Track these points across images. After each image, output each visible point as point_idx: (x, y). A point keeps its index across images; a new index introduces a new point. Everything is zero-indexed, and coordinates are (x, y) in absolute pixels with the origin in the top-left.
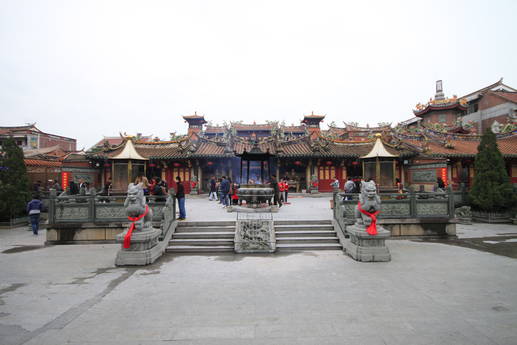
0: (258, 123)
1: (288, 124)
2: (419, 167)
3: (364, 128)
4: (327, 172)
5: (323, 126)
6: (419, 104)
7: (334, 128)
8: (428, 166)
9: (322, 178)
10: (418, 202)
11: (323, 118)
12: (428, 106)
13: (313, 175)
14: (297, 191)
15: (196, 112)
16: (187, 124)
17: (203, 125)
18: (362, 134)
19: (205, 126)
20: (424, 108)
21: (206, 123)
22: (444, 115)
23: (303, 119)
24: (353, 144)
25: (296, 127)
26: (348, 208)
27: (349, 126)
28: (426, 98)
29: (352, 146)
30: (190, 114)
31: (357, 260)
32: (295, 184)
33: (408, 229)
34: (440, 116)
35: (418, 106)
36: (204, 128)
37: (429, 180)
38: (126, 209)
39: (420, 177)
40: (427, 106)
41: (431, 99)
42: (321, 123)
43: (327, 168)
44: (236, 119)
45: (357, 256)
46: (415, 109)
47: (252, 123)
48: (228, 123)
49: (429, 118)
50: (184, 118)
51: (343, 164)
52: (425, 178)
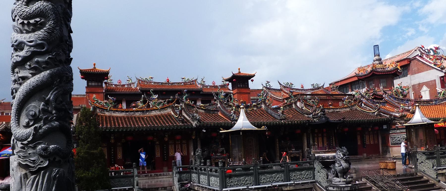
0: (172, 81)
2: (398, 131)
3: (299, 90)
5: (252, 85)
15: (239, 69)
23: (230, 76)
39: (399, 140)
44: (145, 76)
47: (164, 81)
48: (134, 80)
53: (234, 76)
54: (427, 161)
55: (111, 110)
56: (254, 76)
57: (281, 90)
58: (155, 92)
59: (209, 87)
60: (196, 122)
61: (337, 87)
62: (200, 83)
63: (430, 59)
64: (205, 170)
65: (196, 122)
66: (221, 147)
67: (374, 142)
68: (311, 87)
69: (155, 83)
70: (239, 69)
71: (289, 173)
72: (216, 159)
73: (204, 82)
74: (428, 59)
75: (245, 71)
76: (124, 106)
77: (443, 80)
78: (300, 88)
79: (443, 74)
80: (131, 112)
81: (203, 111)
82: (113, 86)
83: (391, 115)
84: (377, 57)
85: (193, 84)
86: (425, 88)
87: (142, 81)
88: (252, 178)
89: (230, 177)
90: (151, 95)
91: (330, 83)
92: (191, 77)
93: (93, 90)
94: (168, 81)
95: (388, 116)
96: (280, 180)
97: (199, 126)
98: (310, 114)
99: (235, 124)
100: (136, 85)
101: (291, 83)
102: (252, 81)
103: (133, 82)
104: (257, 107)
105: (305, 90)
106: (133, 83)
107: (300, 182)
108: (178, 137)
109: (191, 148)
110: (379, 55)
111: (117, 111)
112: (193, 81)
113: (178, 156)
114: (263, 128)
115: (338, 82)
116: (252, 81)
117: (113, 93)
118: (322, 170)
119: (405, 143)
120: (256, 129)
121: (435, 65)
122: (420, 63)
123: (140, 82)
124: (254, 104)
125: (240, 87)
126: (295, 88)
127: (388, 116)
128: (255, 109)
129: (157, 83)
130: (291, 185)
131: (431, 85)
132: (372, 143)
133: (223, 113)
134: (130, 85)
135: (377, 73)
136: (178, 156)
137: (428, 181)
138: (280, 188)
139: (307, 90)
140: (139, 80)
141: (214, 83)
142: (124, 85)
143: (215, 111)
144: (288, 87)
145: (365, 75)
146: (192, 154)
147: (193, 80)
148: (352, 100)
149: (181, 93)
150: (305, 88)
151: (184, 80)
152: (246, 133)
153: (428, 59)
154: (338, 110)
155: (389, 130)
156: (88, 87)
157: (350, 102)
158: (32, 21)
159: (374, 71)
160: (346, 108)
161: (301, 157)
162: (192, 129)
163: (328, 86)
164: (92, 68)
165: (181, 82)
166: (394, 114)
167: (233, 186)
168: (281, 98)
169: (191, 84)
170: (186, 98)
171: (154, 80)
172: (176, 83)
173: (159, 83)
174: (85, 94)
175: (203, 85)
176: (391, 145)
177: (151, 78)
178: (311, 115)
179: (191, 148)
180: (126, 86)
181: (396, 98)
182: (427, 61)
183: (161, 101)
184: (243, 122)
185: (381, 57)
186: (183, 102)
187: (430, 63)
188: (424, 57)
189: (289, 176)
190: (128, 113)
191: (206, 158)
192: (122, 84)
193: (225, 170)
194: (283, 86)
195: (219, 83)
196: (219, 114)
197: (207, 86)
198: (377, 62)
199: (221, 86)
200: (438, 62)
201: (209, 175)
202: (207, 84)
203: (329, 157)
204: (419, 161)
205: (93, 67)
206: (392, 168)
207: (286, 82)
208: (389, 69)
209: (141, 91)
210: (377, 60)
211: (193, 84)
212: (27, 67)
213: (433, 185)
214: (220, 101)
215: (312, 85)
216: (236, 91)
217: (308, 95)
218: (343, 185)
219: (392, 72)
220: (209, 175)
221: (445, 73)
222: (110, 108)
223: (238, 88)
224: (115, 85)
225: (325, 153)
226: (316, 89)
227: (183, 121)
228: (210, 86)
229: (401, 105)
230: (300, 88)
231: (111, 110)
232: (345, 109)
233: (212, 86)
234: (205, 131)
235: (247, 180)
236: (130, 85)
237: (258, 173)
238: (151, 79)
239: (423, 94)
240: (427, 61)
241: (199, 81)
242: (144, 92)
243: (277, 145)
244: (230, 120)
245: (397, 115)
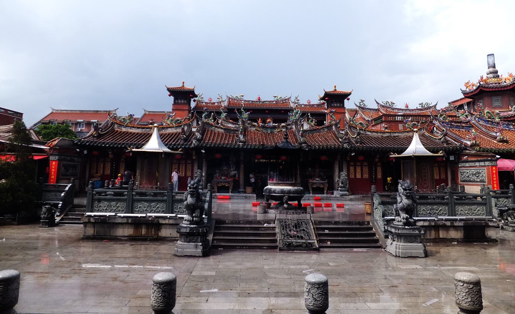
0: (263, 99)
1: (303, 101)
2: (467, 165)
3: (402, 110)
4: (359, 170)
5: (349, 104)
6: (468, 83)
7: (363, 108)
8: (477, 164)
9: (352, 176)
10: (456, 204)
11: (350, 94)
12: (479, 86)
13: (342, 173)
14: (325, 192)
15: (183, 83)
16: (172, 98)
17: (192, 100)
18: (400, 118)
19: (194, 101)
20: (475, 88)
21: (196, 96)
22: (499, 98)
23: (322, 95)
24: (389, 134)
25: (313, 105)
26: (386, 209)
27: (383, 106)
28: (476, 74)
29: (388, 137)
30: (176, 84)
31: (396, 256)
32: (323, 184)
33: (448, 233)
34: (494, 98)
35: (467, 84)
36: (193, 105)
37: (479, 180)
38: (185, 203)
39: (468, 177)
40: (478, 84)
41: (482, 78)
42: (346, 101)
43: (359, 164)
44: (235, 94)
45: (396, 251)
46: (464, 88)
47: (255, 99)
48: (224, 98)
49: (482, 101)
50: (169, 90)
51: (377, 160)
52: (475, 178)
56: (350, 94)
58: (247, 110)
62: (293, 101)
67: (440, 177)
69: (245, 101)
70: (183, 83)
71: (455, 206)
72: (219, 182)
75: (341, 89)
78: (404, 107)
81: (222, 131)
82: (204, 104)
83: (462, 143)
84: (491, 70)
85: (286, 102)
89: (99, 201)
91: (450, 101)
92: (282, 95)
93: (179, 107)
94: (259, 100)
95: (458, 144)
96: (160, 211)
97: (198, 146)
101: (392, 102)
102: (348, 99)
103: (223, 100)
104: (287, 128)
105: (409, 110)
106: (223, 101)
107: (429, 218)
110: (494, 67)
111: (133, 127)
113: (175, 176)
114: (440, 154)
115: (458, 101)
116: (348, 99)
118: (379, 207)
120: (431, 154)
126: (396, 107)
127: (458, 144)
128: (284, 130)
130: (171, 218)
132: (359, 176)
135: (486, 90)
136: (175, 176)
137: (374, 235)
138: (156, 220)
139: (413, 110)
140: (230, 98)
142: (214, 103)
143: (236, 130)
145: (472, 92)
148: (418, 122)
151: (276, 98)
152: (418, 159)
154: (396, 135)
155: (458, 163)
156: (175, 103)
159: (482, 86)
160: (408, 132)
161: (326, 189)
163: (448, 105)
164: (181, 86)
165: (273, 100)
166: (465, 141)
167: (101, 211)
169: (283, 103)
170: (205, 117)
171: (245, 98)
174: (171, 111)
176: (460, 183)
180: (216, 104)
181: (489, 121)
184: (416, 147)
185: (497, 68)
189: (455, 209)
192: (212, 102)
193: (174, 194)
194: (381, 105)
197: (301, 105)
198: (491, 75)
203: (276, 190)
205: (334, 89)
206: (369, 212)
208: (505, 84)
210: (491, 73)
211: (286, 102)
213: (377, 241)
215: (420, 104)
217: (399, 115)
218: (400, 227)
219: (508, 88)
224: (206, 103)
225: (275, 185)
226: (425, 109)
227: (448, 144)
228: (305, 105)
229: (473, 131)
232: (406, 134)
234: (352, 155)
235: (119, 207)
236: (220, 103)
237: (454, 203)
241: (293, 99)
242: (233, 111)
243: (53, 170)
245: (469, 143)
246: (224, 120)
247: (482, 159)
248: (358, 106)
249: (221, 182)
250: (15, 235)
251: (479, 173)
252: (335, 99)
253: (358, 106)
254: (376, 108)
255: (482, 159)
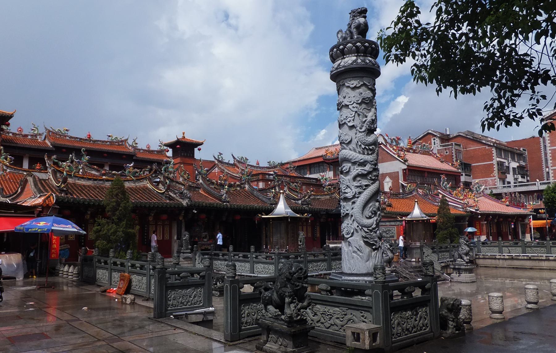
0: (95, 137)
5: (198, 154)
8: (388, 224)
15: (184, 133)
23: (173, 139)
44: (57, 127)
47: (84, 136)
48: (42, 130)
53: (178, 142)
54: (433, 255)
55: (76, 176)
56: (201, 144)
57: (234, 165)
59: (141, 151)
60: (187, 201)
61: (294, 167)
62: (131, 144)
63: (393, 149)
64: (106, 263)
65: (187, 201)
66: (205, 232)
68: (267, 165)
69: (71, 137)
70: (184, 133)
73: (136, 144)
74: (391, 149)
75: (191, 137)
76: (26, 165)
77: (405, 173)
79: (405, 167)
80: (101, 180)
82: (11, 135)
85: (122, 145)
86: (388, 179)
87: (54, 133)
88: (497, 248)
90: (82, 155)
94: (90, 138)
97: (191, 205)
98: (298, 200)
99: (276, 207)
100: (43, 137)
102: (199, 150)
103: (40, 132)
104: (241, 187)
105: (260, 168)
106: (40, 134)
108: (165, 217)
109: (175, 231)
112: (122, 141)
115: (296, 162)
116: (199, 150)
117: (13, 145)
119: (403, 237)
121: (399, 156)
122: (384, 152)
123: (51, 134)
124: (238, 183)
125: (184, 156)
126: (250, 164)
129: (74, 138)
131: (394, 176)
133: (205, 190)
134: (36, 136)
139: (263, 168)
140: (49, 131)
141: (149, 147)
142: (26, 136)
143: (196, 187)
144: (242, 162)
145: (333, 159)
146: (175, 238)
147: (123, 139)
149: (78, 152)
150: (261, 165)
151: (110, 138)
153: (391, 149)
154: (318, 197)
157: (330, 189)
158: (371, 147)
160: (326, 195)
162: (180, 208)
165: (107, 140)
168: (237, 175)
169: (119, 145)
171: (70, 134)
172: (100, 141)
173: (77, 138)
175: (135, 148)
177: (67, 130)
178: (300, 202)
179: (175, 231)
180: (29, 137)
182: (391, 151)
183: (136, 170)
184: (282, 208)
186: (162, 174)
187: (394, 153)
188: (388, 146)
190: (96, 182)
191: (193, 242)
192: (23, 133)
195: (155, 147)
196: (201, 191)
197: (140, 150)
199: (157, 151)
200: (402, 153)
201: (111, 269)
202: (139, 147)
204: (426, 255)
205: (182, 136)
207: (240, 156)
209: (54, 146)
211: (122, 145)
212: (369, 178)
214: (202, 177)
216: (178, 160)
220: (111, 269)
221: (408, 166)
222: (74, 174)
223: (181, 156)
224: (13, 134)
228: (144, 150)
230: (255, 165)
231: (76, 176)
232: (324, 197)
233: (145, 150)
234: (196, 212)
238: (67, 132)
239: (385, 184)
240: (391, 151)
241: (130, 142)
244: (220, 200)
246: (86, 165)
247: (392, 220)
248: (216, 159)
249: (204, 245)
250: (543, 265)
251: (389, 231)
252: (184, 148)
253: (216, 159)
254: (232, 162)
255: (392, 220)
